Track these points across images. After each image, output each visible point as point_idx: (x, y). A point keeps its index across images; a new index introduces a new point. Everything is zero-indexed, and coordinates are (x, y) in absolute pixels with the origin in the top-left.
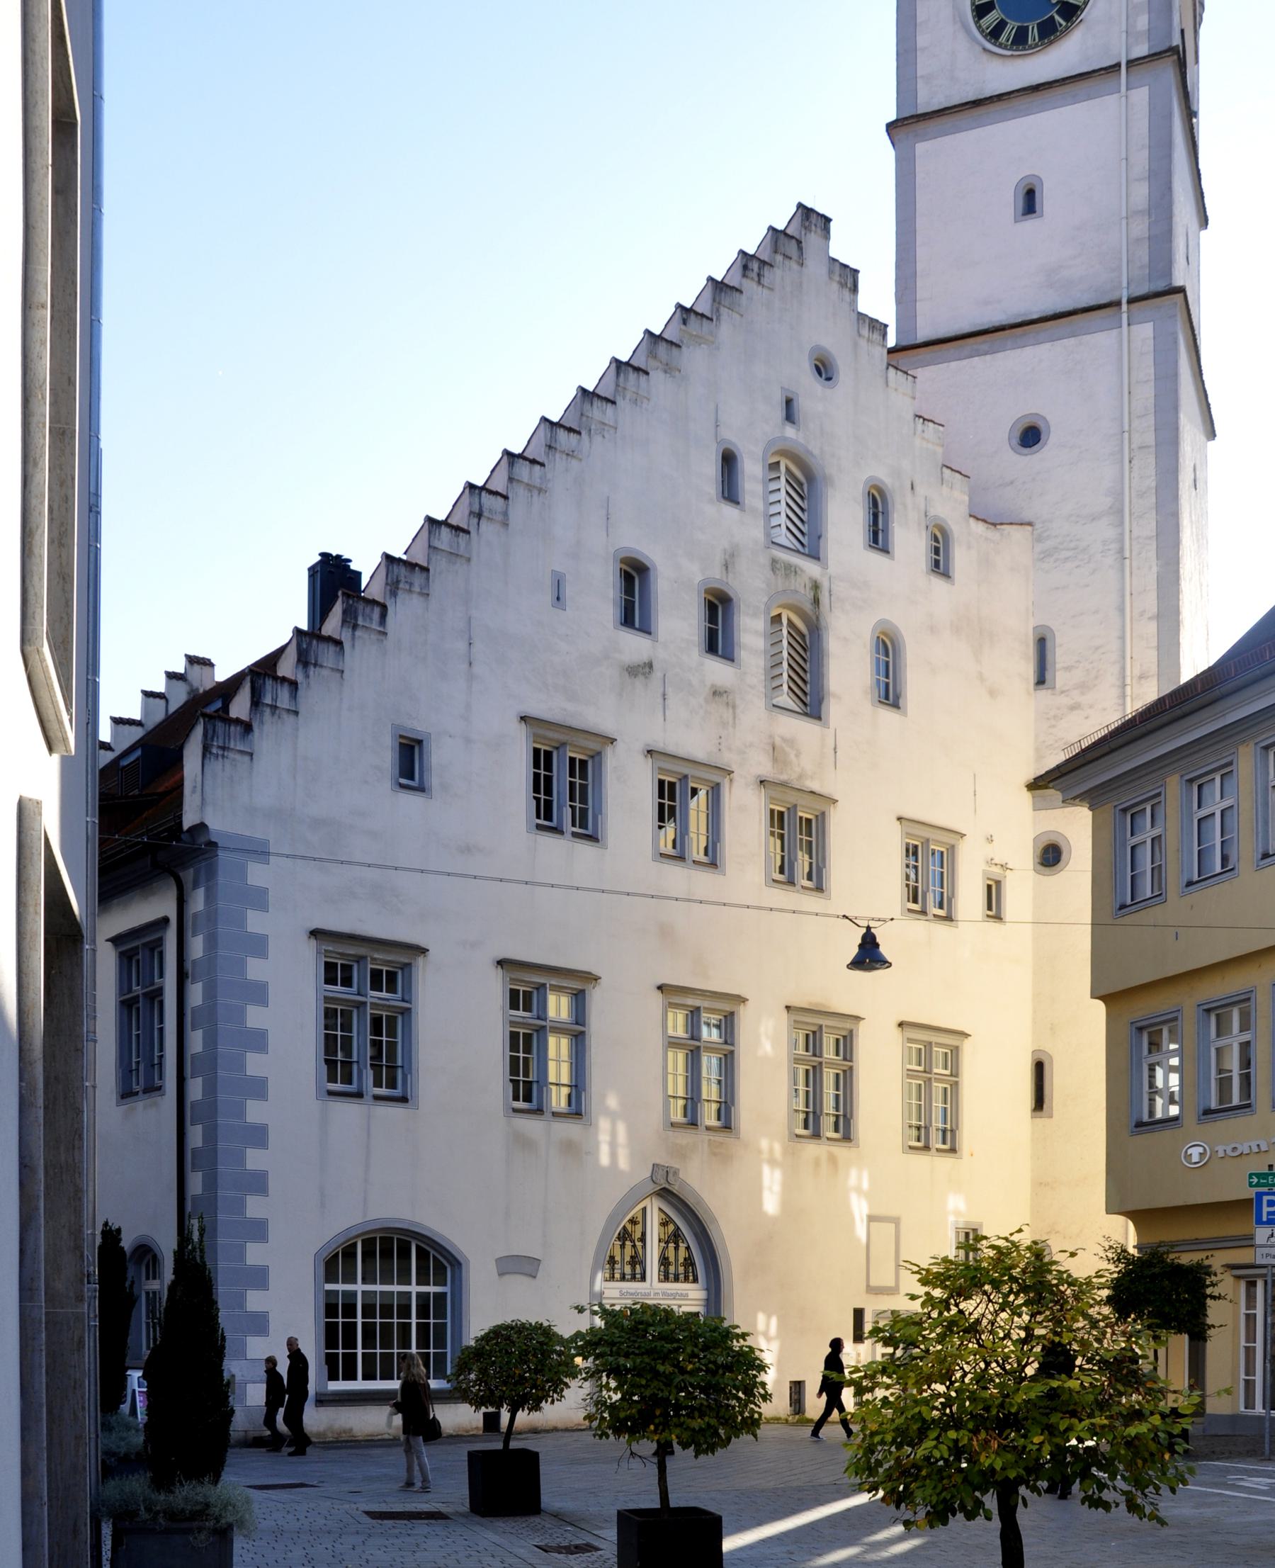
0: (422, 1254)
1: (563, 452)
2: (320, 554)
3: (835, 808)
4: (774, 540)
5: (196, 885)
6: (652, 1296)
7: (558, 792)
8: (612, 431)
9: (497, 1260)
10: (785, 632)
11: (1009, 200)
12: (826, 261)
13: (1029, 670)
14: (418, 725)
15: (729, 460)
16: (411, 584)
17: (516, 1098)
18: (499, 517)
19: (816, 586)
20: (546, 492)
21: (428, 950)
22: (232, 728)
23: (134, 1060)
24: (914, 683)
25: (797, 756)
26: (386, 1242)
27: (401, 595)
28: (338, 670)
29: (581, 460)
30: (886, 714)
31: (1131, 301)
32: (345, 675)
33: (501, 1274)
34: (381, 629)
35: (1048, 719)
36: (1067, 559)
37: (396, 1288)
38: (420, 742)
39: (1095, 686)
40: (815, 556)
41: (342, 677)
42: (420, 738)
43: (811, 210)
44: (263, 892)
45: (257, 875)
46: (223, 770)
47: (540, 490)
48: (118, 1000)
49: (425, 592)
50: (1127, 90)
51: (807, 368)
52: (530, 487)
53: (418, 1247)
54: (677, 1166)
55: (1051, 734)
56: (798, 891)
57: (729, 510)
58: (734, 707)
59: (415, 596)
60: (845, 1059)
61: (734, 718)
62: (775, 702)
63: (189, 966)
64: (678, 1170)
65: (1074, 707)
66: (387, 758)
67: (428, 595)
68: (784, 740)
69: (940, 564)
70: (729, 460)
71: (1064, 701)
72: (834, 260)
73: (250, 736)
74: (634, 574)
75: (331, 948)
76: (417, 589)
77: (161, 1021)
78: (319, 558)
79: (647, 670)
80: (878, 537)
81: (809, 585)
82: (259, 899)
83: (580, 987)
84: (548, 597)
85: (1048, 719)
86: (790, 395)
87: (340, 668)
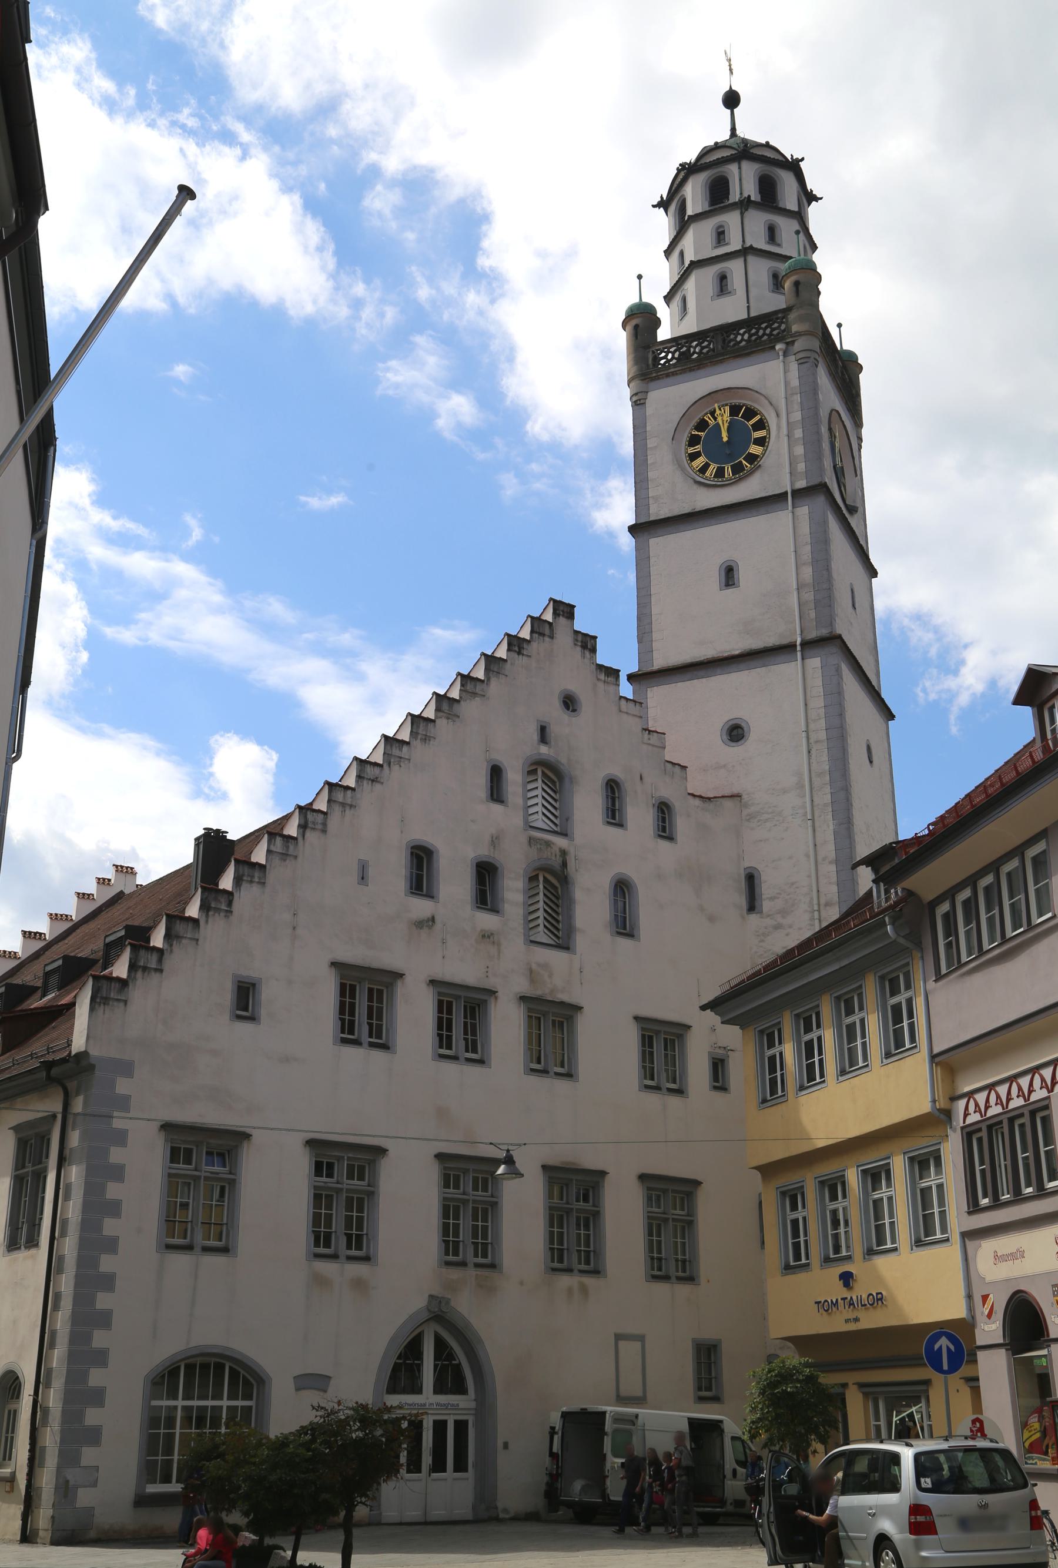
0: (234, 1374)
1: (367, 779)
2: (204, 829)
3: (581, 1013)
4: (531, 824)
5: (78, 1094)
6: (427, 1407)
7: (359, 1013)
8: (406, 762)
9: (294, 1378)
10: (541, 886)
11: (715, 577)
12: (572, 633)
13: (743, 901)
14: (251, 971)
15: (496, 773)
16: (253, 877)
17: (441, 1047)
18: (320, 827)
19: (564, 853)
20: (355, 807)
21: (251, 1135)
22: (113, 984)
23: (21, 1220)
24: (646, 917)
25: (551, 976)
26: (205, 1367)
27: (245, 886)
28: (194, 939)
29: (382, 783)
30: (624, 942)
31: (805, 644)
32: (199, 943)
33: (298, 1389)
34: (229, 909)
35: (758, 936)
36: (766, 820)
37: (210, 1403)
38: (254, 985)
39: (792, 911)
40: (564, 834)
41: (197, 944)
42: (254, 982)
43: (561, 602)
44: (127, 1098)
45: (123, 1086)
46: (104, 1013)
47: (351, 806)
48: (14, 1174)
49: (263, 881)
50: (793, 508)
51: (557, 703)
52: (343, 805)
53: (230, 1368)
54: (449, 1297)
55: (761, 947)
56: (551, 1077)
57: (497, 808)
58: (499, 945)
59: (254, 885)
60: (594, 1205)
61: (499, 953)
62: (532, 938)
63: (67, 1152)
64: (450, 1299)
65: (778, 927)
66: (228, 997)
67: (264, 883)
68: (539, 965)
69: (665, 828)
70: (496, 773)
71: (769, 922)
72: (579, 632)
73: (126, 989)
74: (423, 855)
75: (176, 1137)
76: (256, 880)
77: (44, 1191)
78: (203, 832)
79: (430, 923)
80: (614, 815)
81: (558, 853)
82: (124, 1103)
83: (372, 1158)
84: (355, 877)
85: (758, 936)
86: (544, 724)
87: (196, 937)
